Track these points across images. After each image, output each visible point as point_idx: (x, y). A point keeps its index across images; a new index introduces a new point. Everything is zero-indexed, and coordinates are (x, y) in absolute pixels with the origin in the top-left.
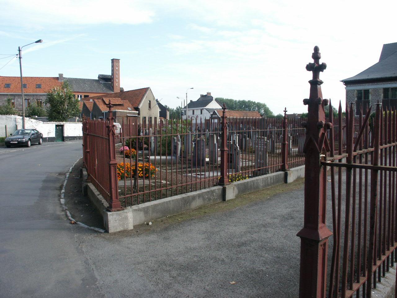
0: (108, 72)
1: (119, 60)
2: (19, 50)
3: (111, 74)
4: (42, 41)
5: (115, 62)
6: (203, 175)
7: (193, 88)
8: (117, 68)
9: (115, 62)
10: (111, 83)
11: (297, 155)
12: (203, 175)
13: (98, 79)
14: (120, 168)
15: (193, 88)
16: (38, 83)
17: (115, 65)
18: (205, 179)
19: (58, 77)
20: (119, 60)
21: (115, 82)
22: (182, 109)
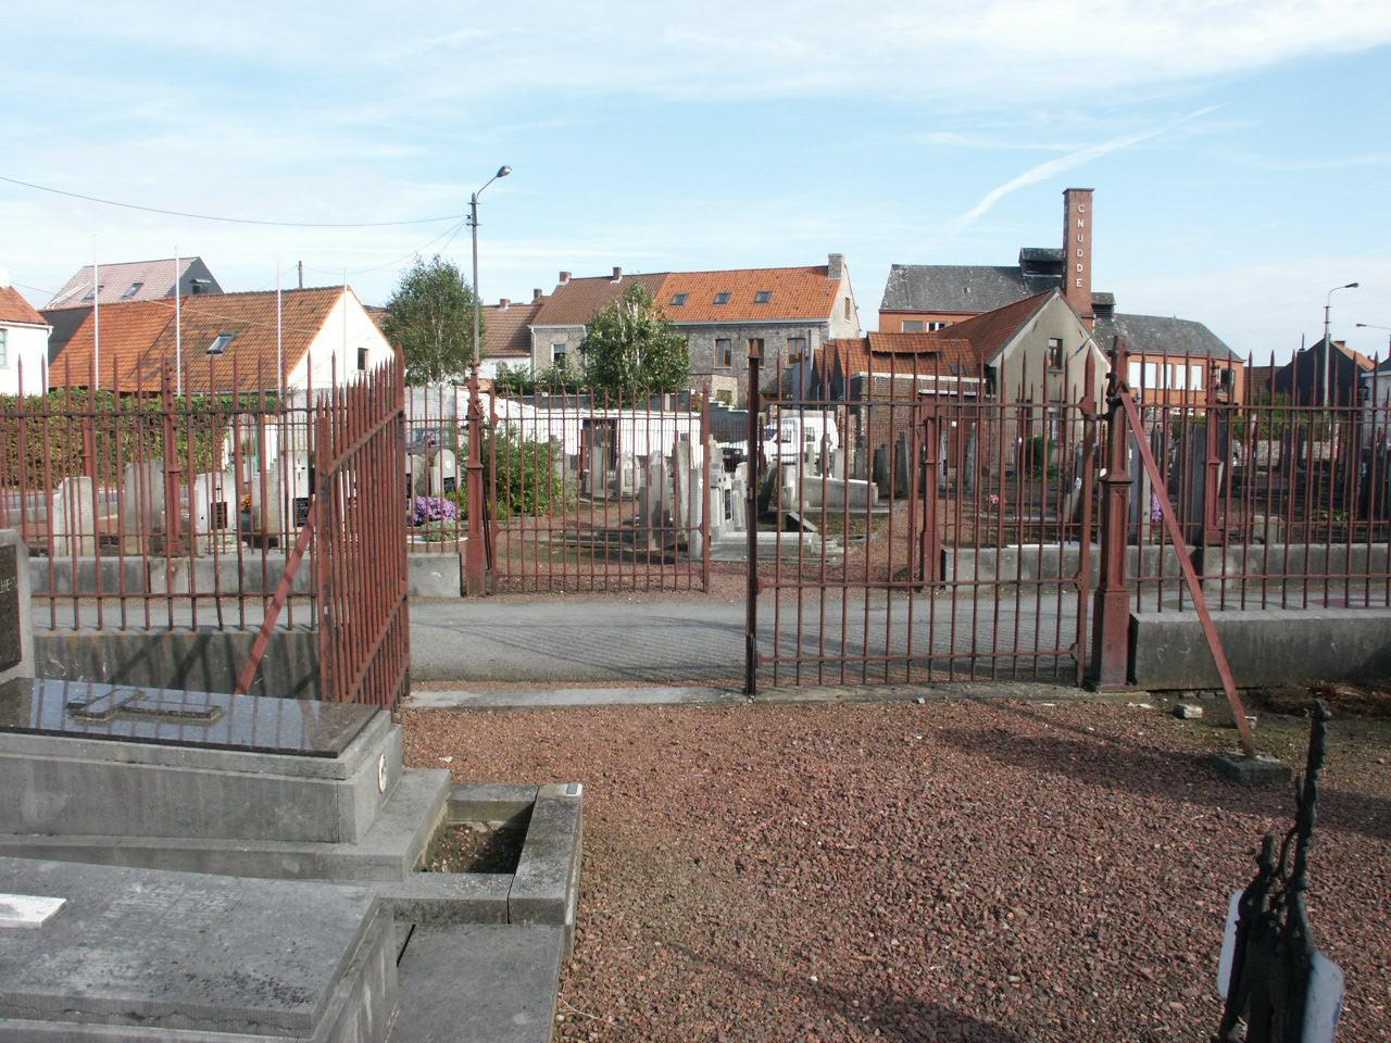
0: (1050, 239)
1: (1092, 190)
2: (474, 204)
3: (1060, 246)
4: (507, 170)
5: (1076, 200)
6: (241, 394)
7: (1355, 285)
8: (1081, 223)
9: (1076, 200)
10: (1060, 276)
11: (407, 385)
12: (241, 394)
13: (1018, 265)
14: (485, 427)
15: (1355, 285)
16: (764, 289)
17: (1072, 210)
18: (1285, 573)
19: (827, 264)
20: (1092, 190)
21: (1070, 273)
22: (1363, 375)
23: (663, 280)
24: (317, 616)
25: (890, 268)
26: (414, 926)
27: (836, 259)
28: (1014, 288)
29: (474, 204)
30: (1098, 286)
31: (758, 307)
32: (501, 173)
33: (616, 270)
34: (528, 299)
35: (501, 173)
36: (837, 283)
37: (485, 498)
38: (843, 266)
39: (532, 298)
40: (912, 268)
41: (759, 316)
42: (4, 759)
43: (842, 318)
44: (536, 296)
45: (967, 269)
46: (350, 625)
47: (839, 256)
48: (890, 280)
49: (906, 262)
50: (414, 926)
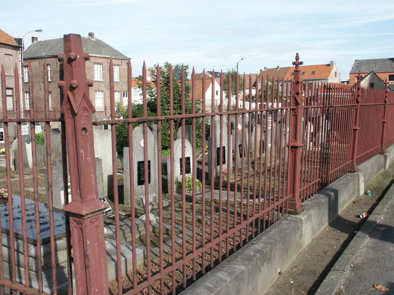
2: (237, 64)
16: (314, 71)
23: (289, 69)
24: (320, 135)
25: (355, 61)
26: (5, 54)
27: (332, 62)
28: (391, 64)
29: (237, 64)
30: (149, 160)
31: (312, 75)
32: (242, 59)
33: (278, 67)
34: (258, 73)
35: (242, 59)
36: (332, 68)
37: (231, 129)
38: (334, 64)
39: (260, 72)
40: (361, 60)
41: (312, 77)
42: (1, 161)
43: (334, 77)
44: (261, 71)
45: (377, 60)
46: (335, 146)
47: (333, 61)
48: (354, 64)
49: (359, 58)
50: (5, 54)
